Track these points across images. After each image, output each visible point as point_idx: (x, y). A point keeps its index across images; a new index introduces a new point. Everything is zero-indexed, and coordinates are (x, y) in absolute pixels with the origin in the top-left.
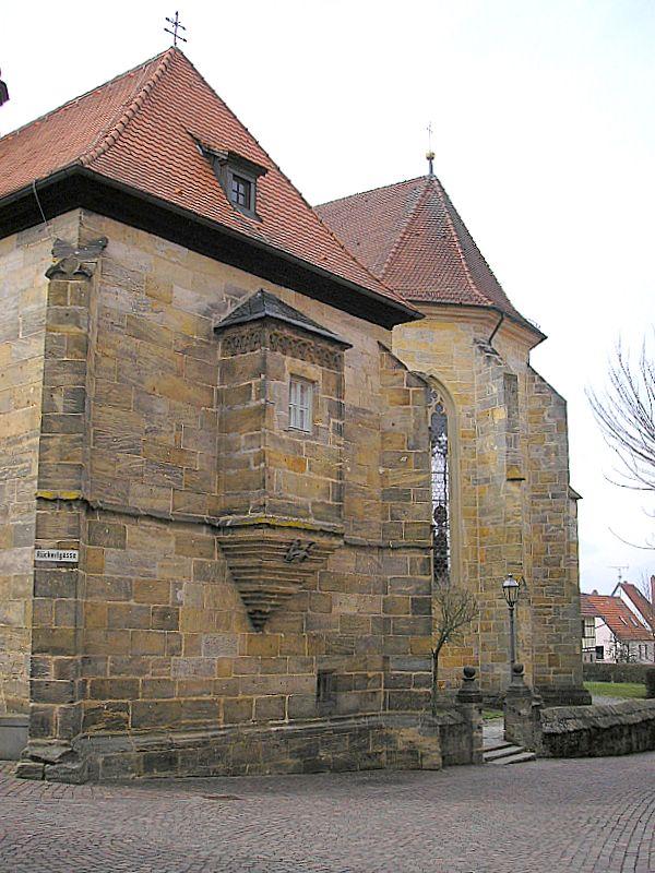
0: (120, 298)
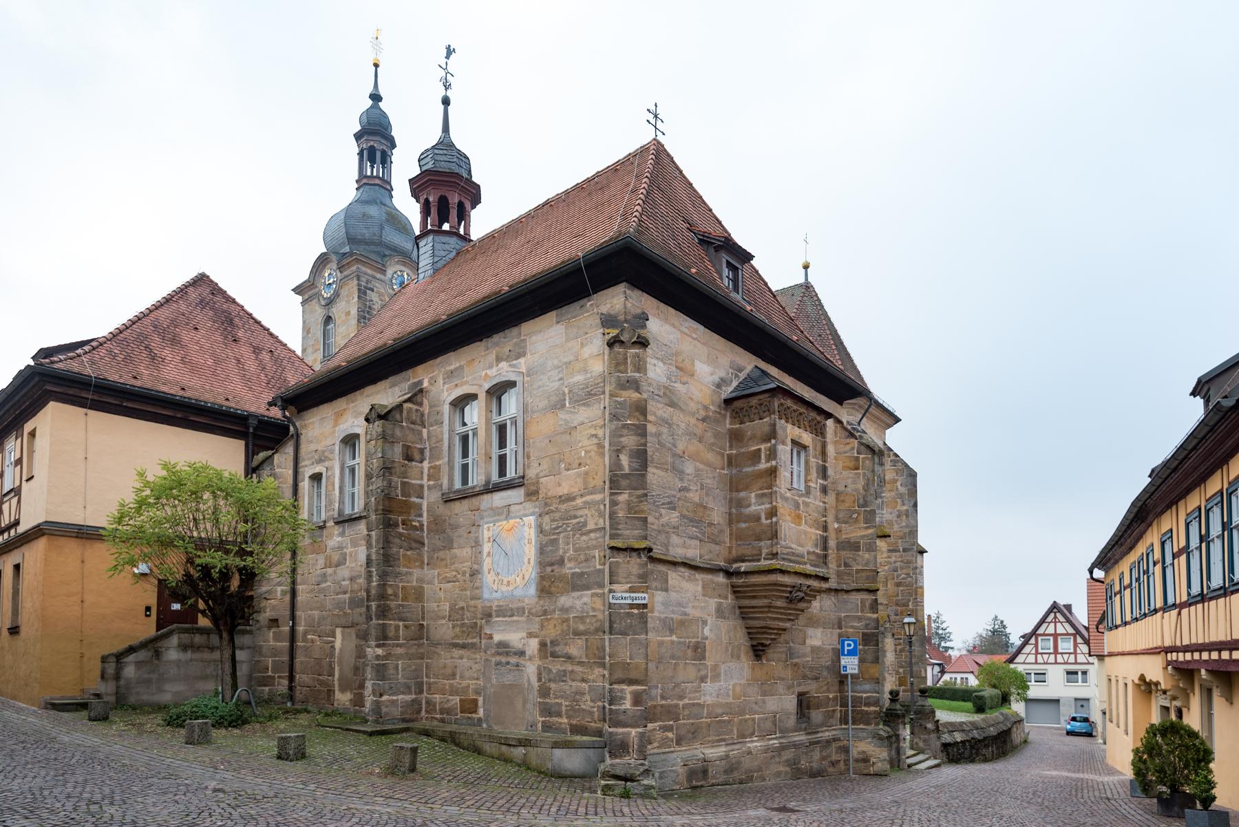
0: (658, 370)
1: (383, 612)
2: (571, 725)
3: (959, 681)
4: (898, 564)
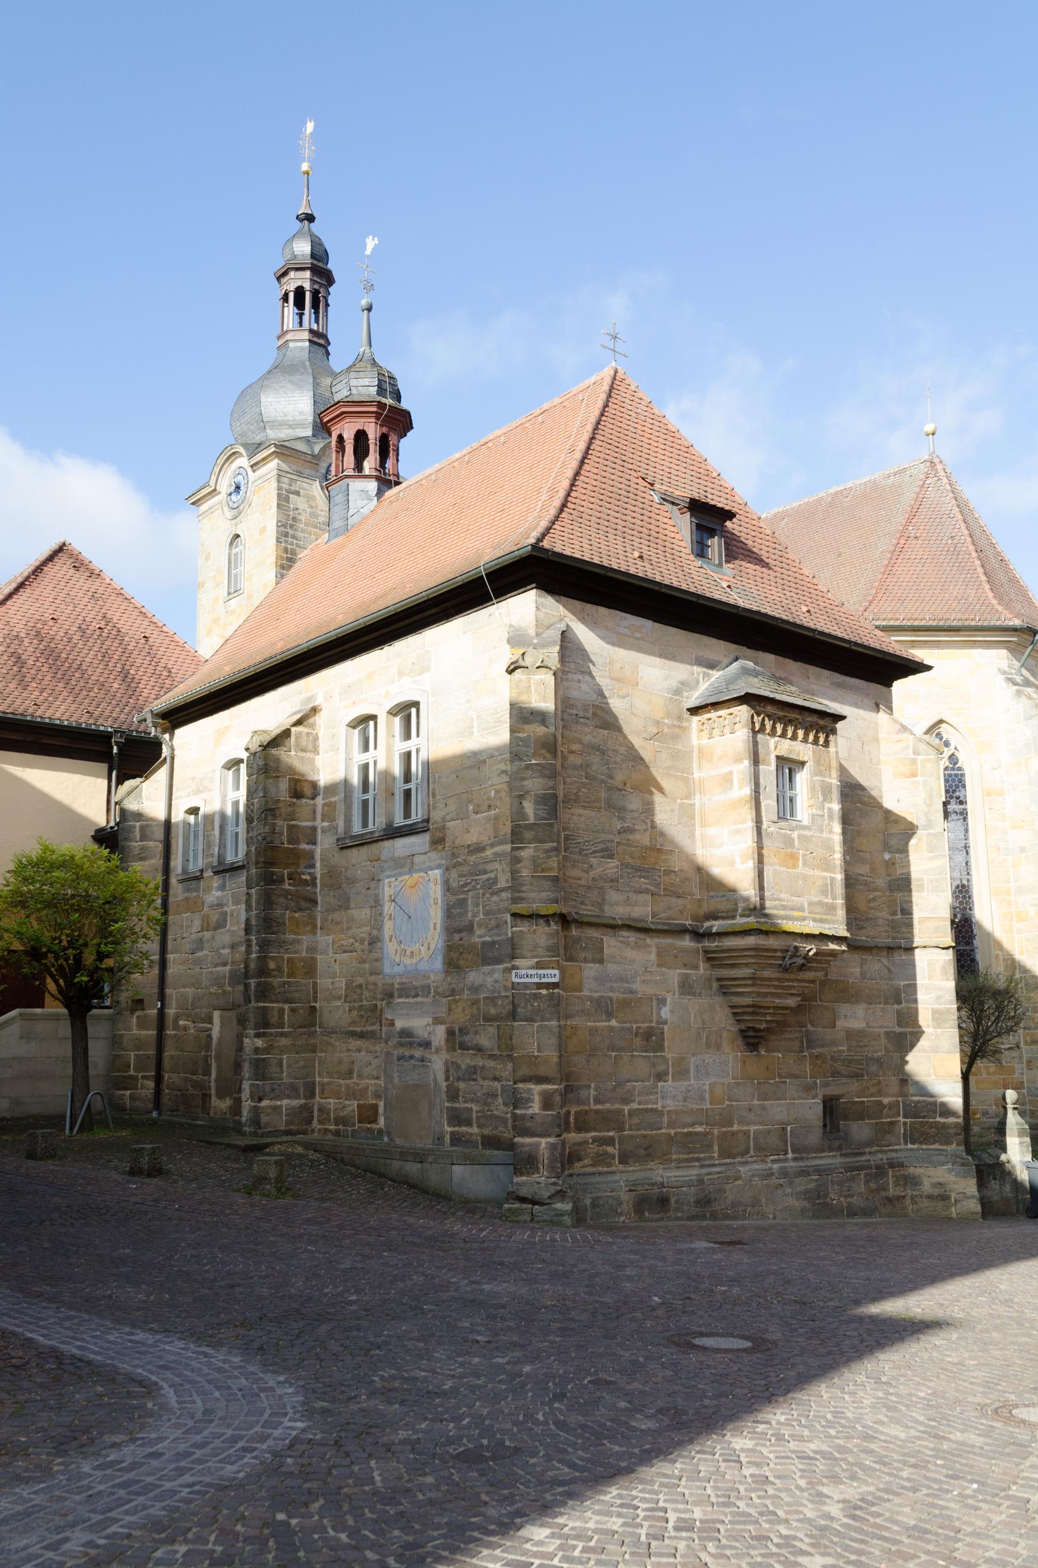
1: (264, 992)
2: (483, 1137)
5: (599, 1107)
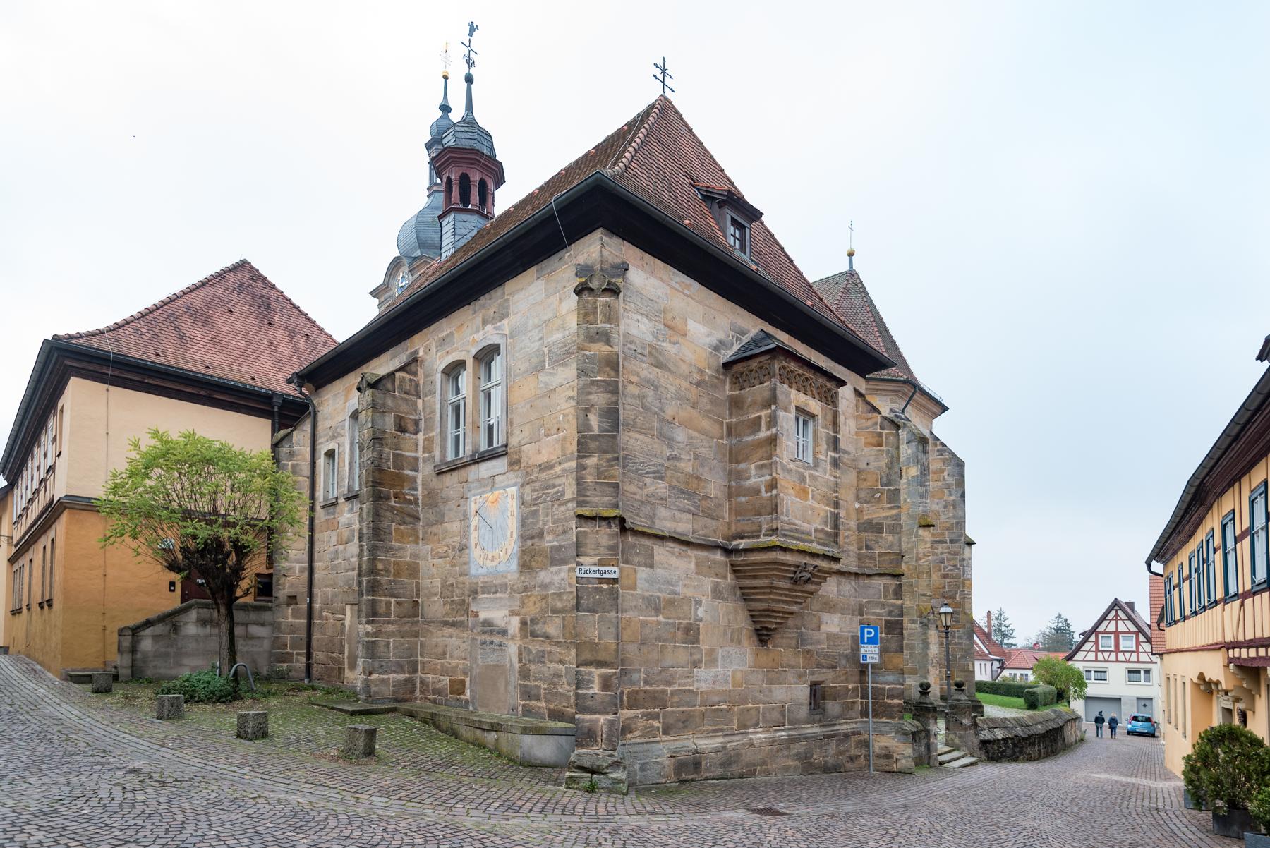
1: (374, 588)
2: (549, 710)
3: (1018, 677)
4: (945, 556)
5: (648, 688)
